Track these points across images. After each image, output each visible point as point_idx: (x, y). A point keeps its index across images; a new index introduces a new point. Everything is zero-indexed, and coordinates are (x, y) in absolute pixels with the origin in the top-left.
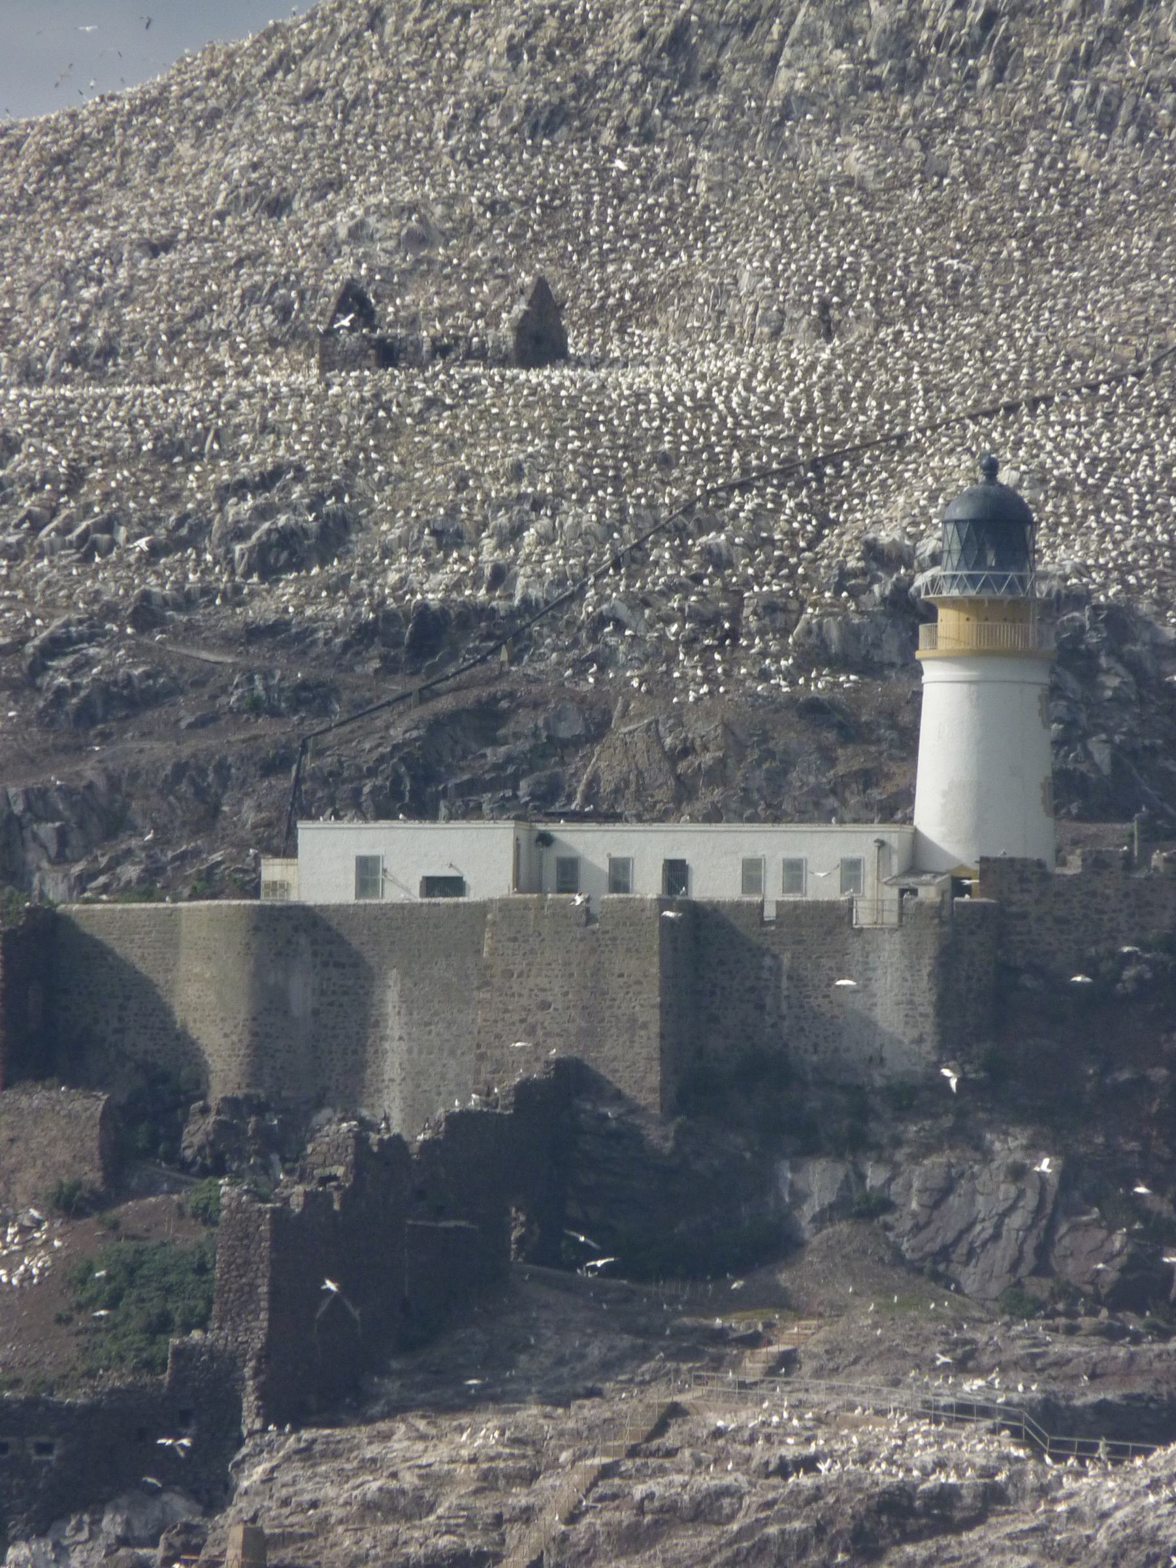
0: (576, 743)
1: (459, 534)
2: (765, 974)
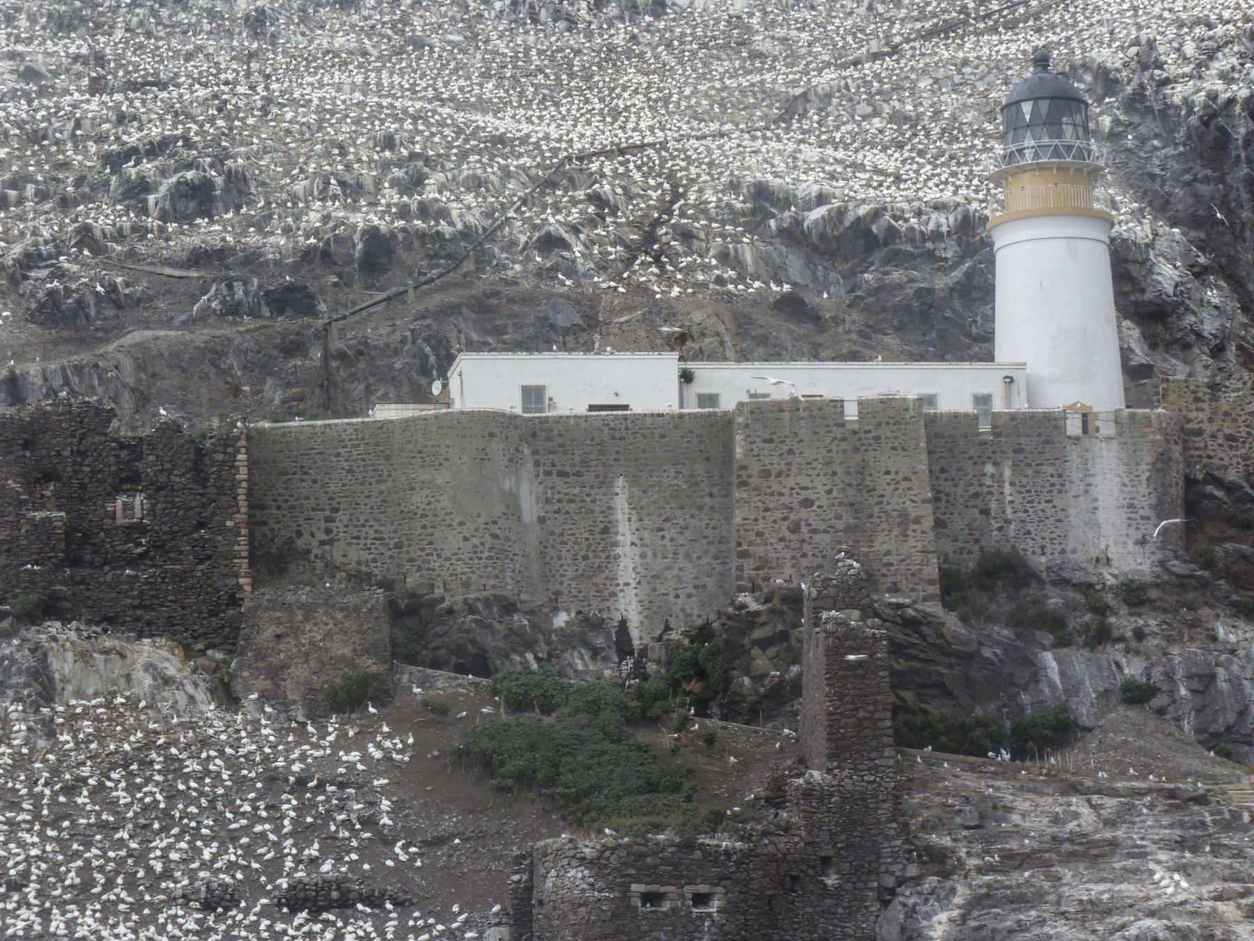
2: (988, 481)
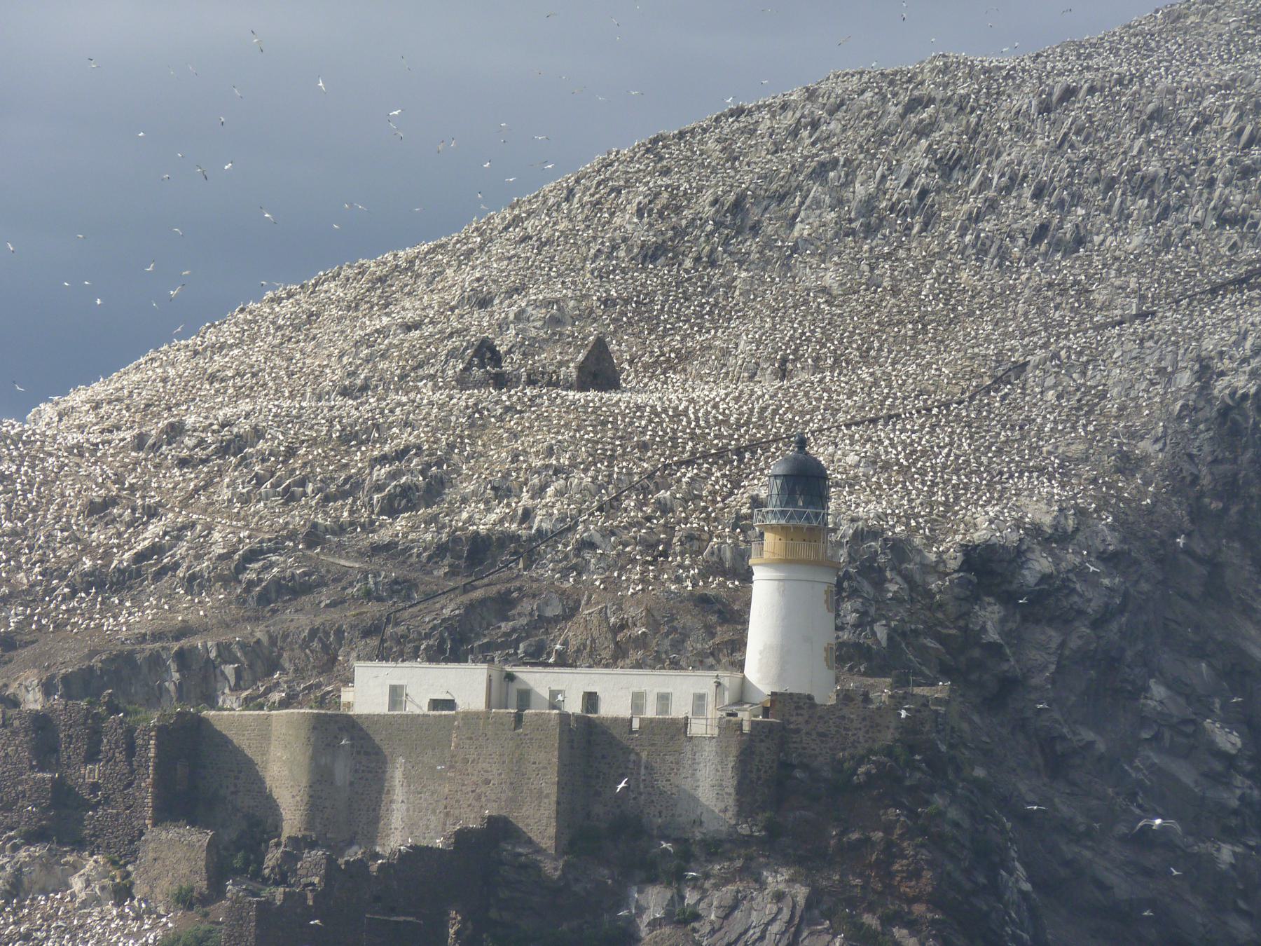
0: (556, 620)
1: (509, 490)
2: (631, 766)
